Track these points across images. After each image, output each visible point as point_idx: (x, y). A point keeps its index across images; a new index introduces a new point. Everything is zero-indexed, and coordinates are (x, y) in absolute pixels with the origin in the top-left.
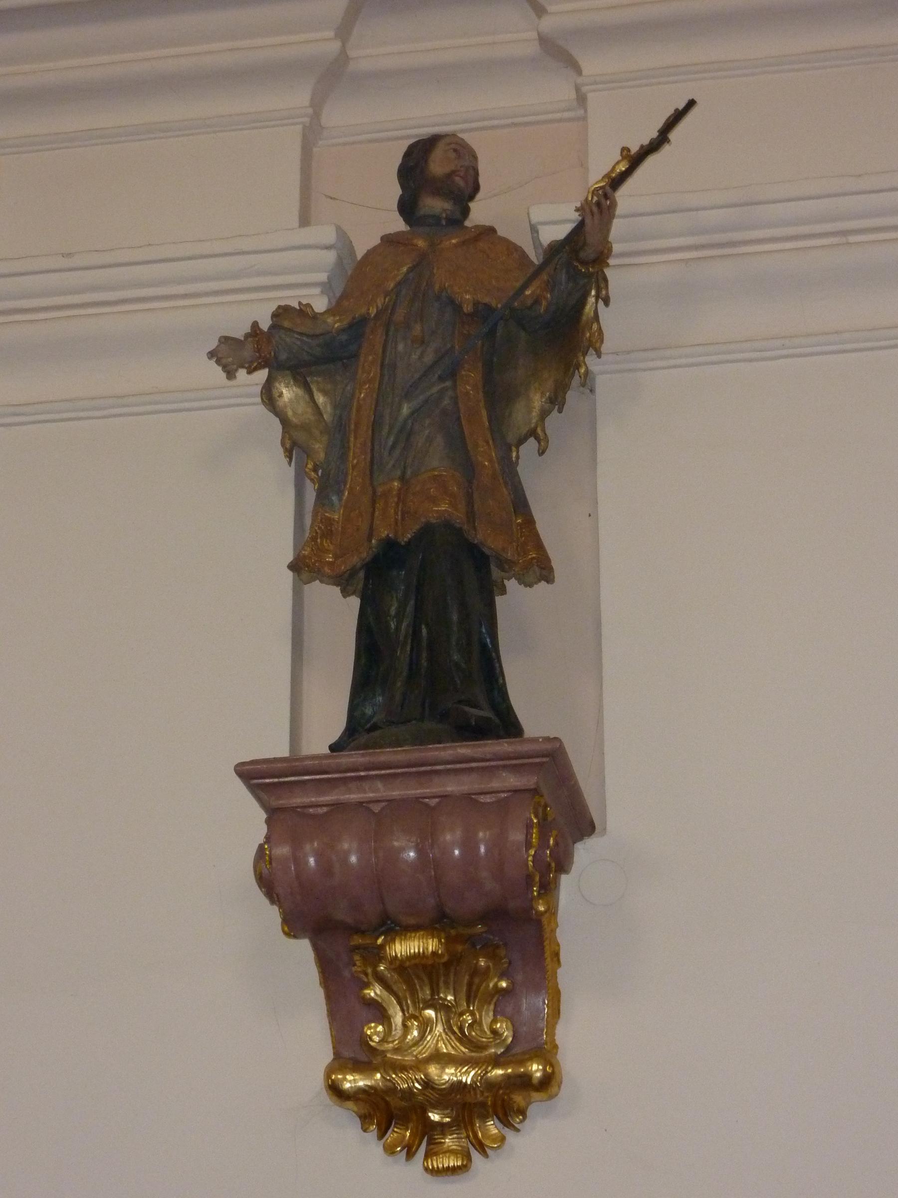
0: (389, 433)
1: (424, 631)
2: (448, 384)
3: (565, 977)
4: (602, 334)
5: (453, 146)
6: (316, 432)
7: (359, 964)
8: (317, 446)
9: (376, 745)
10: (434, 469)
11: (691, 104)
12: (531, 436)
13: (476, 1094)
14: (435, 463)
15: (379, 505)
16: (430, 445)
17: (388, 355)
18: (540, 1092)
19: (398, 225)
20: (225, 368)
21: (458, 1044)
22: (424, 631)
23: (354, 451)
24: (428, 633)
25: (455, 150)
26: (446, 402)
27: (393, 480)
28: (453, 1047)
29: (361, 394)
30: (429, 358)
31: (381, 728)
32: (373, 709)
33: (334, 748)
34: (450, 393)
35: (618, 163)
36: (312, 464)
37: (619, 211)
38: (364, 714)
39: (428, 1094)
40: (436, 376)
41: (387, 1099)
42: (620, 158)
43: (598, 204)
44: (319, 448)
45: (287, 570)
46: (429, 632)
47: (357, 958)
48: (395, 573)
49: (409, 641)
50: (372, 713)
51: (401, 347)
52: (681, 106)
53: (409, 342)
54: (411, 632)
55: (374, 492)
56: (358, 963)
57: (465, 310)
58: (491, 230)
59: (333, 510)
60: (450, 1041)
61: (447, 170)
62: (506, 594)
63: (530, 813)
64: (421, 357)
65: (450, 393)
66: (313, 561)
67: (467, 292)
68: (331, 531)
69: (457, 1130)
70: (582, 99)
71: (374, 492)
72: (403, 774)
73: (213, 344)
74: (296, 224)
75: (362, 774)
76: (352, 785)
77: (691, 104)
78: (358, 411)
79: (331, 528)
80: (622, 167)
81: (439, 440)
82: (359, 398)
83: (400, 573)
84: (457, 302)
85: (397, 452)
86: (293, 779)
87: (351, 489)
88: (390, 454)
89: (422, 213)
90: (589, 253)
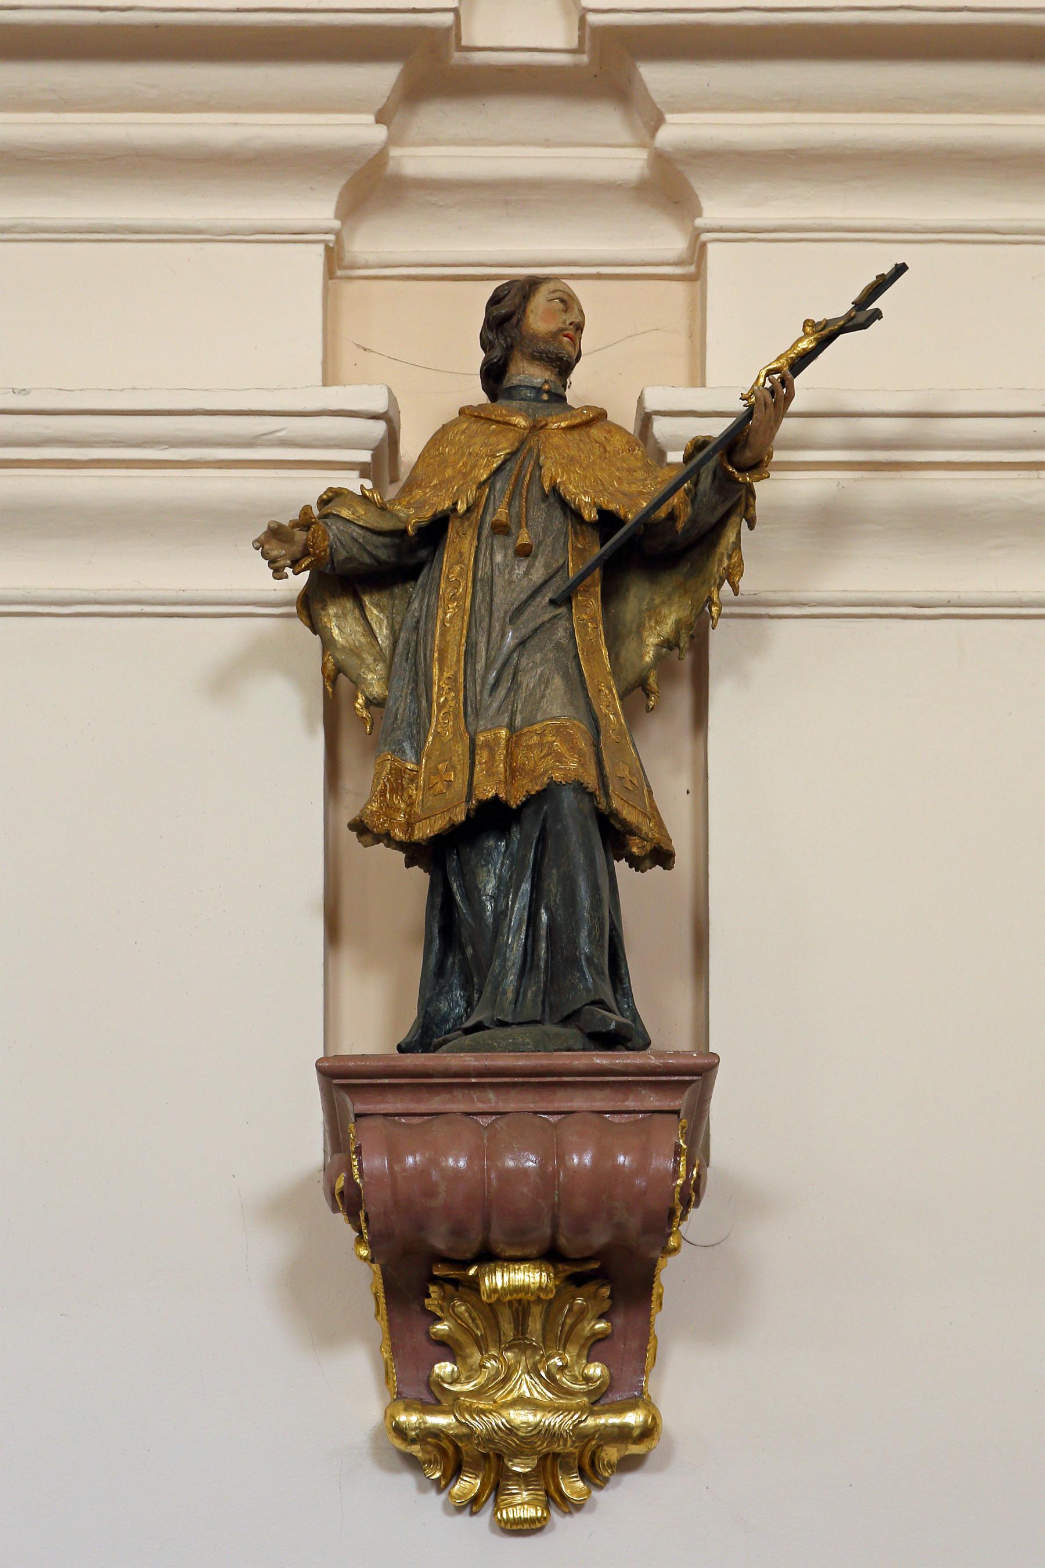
0: (488, 668)
1: (544, 917)
2: (563, 610)
3: (660, 1321)
4: (742, 566)
5: (558, 294)
6: (370, 660)
7: (435, 1297)
8: (370, 676)
9: (491, 1049)
10: (555, 718)
11: (900, 269)
12: (639, 686)
13: (565, 1444)
14: (556, 711)
15: (482, 756)
16: (546, 688)
17: (480, 567)
18: (640, 1444)
19: (480, 397)
20: (272, 562)
21: (545, 1390)
22: (544, 917)
23: (439, 686)
24: (548, 919)
25: (562, 301)
26: (561, 634)
27: (500, 727)
28: (538, 1392)
29: (446, 614)
30: (538, 575)
31: (488, 1028)
32: (449, 1005)
33: (401, 1049)
34: (564, 623)
35: (800, 340)
36: (364, 698)
37: (794, 406)
38: (439, 1010)
39: (509, 1441)
40: (547, 599)
41: (460, 1444)
42: (803, 334)
43: (772, 392)
44: (373, 678)
45: (346, 827)
46: (551, 918)
47: (433, 1289)
48: (491, 843)
49: (524, 927)
50: (447, 1010)
51: (499, 558)
52: (886, 269)
53: (510, 552)
54: (526, 917)
55: (473, 742)
56: (433, 1295)
57: (586, 517)
58: (444, 425)
59: (404, 759)
60: (536, 1385)
61: (553, 327)
62: (407, 868)
63: (679, 1139)
64: (527, 573)
65: (564, 623)
66: (381, 820)
67: (585, 493)
68: (402, 785)
69: (535, 1481)
70: (698, 253)
71: (473, 742)
72: (523, 1084)
73: (260, 531)
74: (321, 383)
75: (473, 1080)
76: (459, 1094)
77: (900, 269)
78: (443, 634)
79: (402, 781)
80: (806, 344)
81: (557, 681)
82: (443, 620)
83: (499, 843)
84: (573, 506)
85: (502, 692)
86: (386, 1081)
87: (437, 734)
88: (490, 695)
89: (515, 381)
90: (748, 455)
